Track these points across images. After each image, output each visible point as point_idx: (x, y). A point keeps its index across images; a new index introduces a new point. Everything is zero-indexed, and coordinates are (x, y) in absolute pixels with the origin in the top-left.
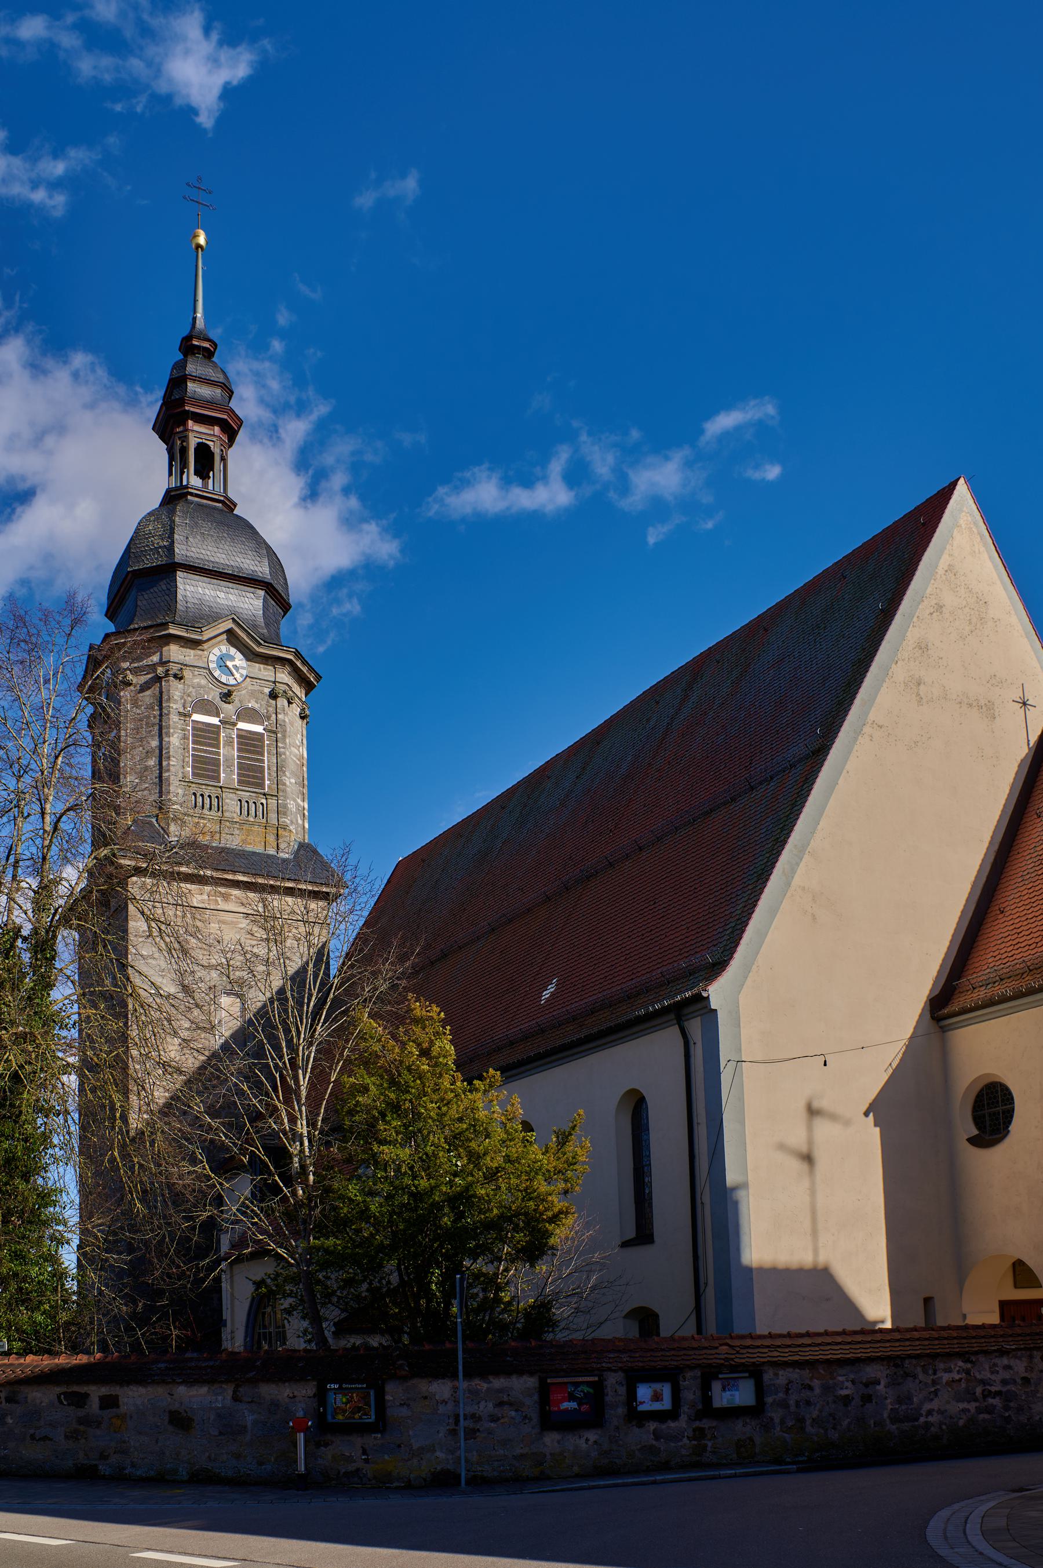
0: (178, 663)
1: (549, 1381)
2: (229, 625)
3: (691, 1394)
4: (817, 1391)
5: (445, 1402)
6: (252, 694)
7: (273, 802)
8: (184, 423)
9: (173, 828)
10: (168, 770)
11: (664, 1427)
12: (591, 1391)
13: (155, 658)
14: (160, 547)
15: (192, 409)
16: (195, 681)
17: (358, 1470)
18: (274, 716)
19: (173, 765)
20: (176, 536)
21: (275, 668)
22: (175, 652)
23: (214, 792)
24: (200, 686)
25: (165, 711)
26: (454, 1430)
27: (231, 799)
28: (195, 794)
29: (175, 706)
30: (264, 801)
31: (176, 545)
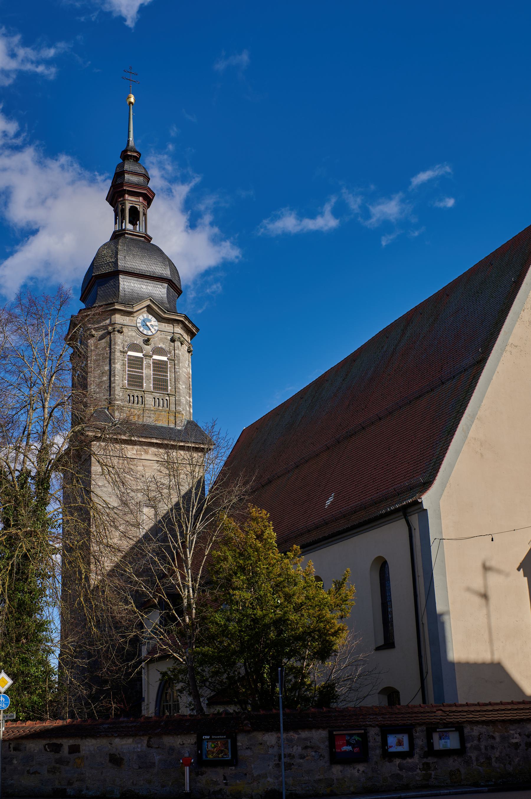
0: (120, 324)
1: (334, 733)
2: (148, 303)
3: (420, 742)
4: (498, 739)
5: (272, 747)
6: (161, 340)
7: (172, 398)
8: (123, 196)
9: (117, 414)
10: (114, 383)
11: (405, 762)
12: (360, 739)
13: (108, 322)
14: (110, 262)
15: (127, 189)
16: (129, 333)
17: (221, 790)
18: (173, 351)
19: (117, 380)
20: (119, 256)
21: (173, 325)
22: (118, 318)
23: (140, 394)
24: (132, 337)
25: (113, 350)
26: (278, 764)
27: (149, 398)
28: (129, 395)
29: (118, 348)
30: (168, 398)
31: (119, 261)
